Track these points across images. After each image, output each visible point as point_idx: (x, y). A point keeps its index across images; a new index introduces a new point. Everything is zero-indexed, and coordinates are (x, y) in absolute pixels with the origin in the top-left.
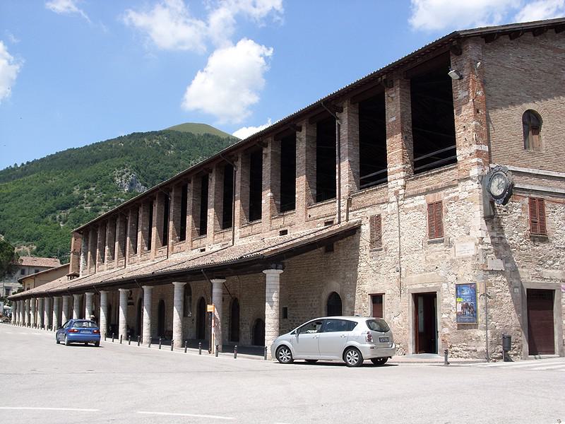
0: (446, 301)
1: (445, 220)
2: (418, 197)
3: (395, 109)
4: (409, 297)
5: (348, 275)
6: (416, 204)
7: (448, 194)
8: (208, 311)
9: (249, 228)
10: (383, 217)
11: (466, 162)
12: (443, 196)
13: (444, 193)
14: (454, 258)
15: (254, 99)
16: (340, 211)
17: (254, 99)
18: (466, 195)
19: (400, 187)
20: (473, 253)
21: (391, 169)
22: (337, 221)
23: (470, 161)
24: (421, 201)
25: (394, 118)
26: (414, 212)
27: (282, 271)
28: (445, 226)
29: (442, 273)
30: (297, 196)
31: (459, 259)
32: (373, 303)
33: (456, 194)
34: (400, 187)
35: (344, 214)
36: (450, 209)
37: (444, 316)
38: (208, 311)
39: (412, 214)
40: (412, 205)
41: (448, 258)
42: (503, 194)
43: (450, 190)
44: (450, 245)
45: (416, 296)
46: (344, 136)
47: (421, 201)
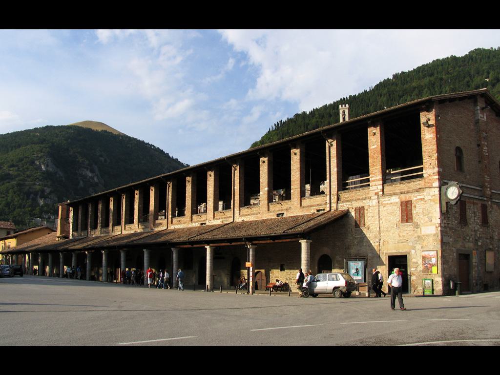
0: (414, 260)
1: (414, 212)
2: (394, 197)
3: (332, 149)
4: (386, 258)
5: (337, 244)
6: (392, 201)
7: (416, 197)
8: (246, 266)
9: (279, 206)
10: (366, 208)
11: (430, 178)
12: (414, 197)
13: (414, 196)
14: (420, 235)
15: (368, 90)
16: (350, 202)
17: (368, 90)
18: (429, 197)
19: (379, 190)
20: (434, 232)
21: (373, 179)
22: (328, 209)
23: (433, 177)
24: (396, 199)
25: (375, 146)
26: (390, 206)
27: (311, 241)
28: (414, 216)
29: (411, 244)
30: (292, 191)
31: (424, 236)
32: (459, 259)
33: (422, 197)
34: (379, 190)
35: (334, 205)
36: (417, 205)
37: (412, 269)
38: (246, 266)
39: (389, 207)
40: (389, 202)
41: (416, 235)
42: (456, 198)
43: (418, 194)
44: (417, 226)
45: (406, 255)
46: (333, 154)
47: (396, 199)
